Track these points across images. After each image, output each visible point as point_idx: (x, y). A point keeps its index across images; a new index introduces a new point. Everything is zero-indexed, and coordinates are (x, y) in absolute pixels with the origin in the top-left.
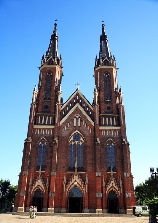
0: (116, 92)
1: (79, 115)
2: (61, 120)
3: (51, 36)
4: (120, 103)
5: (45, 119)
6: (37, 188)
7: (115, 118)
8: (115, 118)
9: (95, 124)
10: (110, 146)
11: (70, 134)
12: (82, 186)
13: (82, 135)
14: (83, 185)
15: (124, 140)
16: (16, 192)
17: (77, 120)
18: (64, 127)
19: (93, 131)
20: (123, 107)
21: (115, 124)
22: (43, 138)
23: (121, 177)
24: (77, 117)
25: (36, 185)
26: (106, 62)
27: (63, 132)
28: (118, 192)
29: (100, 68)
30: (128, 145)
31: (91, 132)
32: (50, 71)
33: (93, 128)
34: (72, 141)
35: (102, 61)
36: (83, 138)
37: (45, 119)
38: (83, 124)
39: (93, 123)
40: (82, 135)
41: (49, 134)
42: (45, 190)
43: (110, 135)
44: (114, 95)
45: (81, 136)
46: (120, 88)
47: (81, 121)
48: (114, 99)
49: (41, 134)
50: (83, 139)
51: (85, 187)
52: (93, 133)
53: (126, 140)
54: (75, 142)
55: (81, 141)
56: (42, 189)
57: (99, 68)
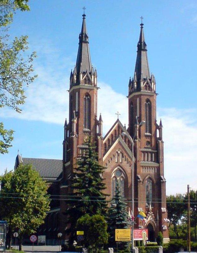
0: (96, 120)
2: (104, 155)
3: (79, 44)
4: (160, 138)
7: (153, 154)
8: (153, 154)
11: (113, 170)
13: (123, 171)
15: (162, 177)
16: (68, 222)
17: (118, 155)
20: (163, 142)
21: (153, 160)
22: (149, 176)
23: (158, 211)
24: (119, 152)
26: (147, 86)
28: (154, 224)
29: (134, 96)
30: (165, 182)
32: (87, 93)
35: (143, 85)
36: (123, 173)
40: (123, 171)
44: (93, 123)
45: (122, 172)
46: (100, 116)
47: (123, 156)
48: (153, 133)
50: (124, 175)
53: (164, 177)
56: (154, 223)
57: (139, 94)
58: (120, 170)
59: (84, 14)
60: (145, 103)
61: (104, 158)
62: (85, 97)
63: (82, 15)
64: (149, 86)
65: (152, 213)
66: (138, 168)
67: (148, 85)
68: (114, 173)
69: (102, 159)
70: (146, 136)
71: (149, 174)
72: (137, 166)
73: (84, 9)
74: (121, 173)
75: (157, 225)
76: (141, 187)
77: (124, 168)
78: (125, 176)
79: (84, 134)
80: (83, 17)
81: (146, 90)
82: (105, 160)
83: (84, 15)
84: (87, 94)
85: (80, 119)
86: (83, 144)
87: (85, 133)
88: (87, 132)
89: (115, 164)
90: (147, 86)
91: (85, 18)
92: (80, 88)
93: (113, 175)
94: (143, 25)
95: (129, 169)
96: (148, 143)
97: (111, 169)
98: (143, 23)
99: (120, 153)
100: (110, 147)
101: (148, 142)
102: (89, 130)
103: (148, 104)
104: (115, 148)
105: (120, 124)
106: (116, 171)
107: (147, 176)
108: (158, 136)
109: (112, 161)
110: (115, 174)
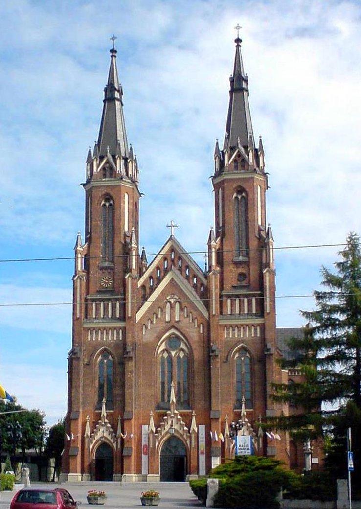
1: (175, 297)
5: (106, 309)
6: (100, 442)
9: (209, 314)
10: (243, 358)
12: (185, 436)
14: (185, 434)
17: (172, 307)
18: (146, 323)
19: (206, 330)
21: (254, 312)
24: (172, 301)
25: (97, 438)
27: (144, 333)
31: (201, 332)
32: (107, 194)
33: (206, 324)
34: (164, 351)
37: (106, 309)
38: (186, 316)
39: (206, 315)
41: (115, 339)
42: (115, 445)
43: (242, 336)
44: (254, 243)
45: (183, 340)
47: (181, 309)
49: (99, 339)
50: (187, 346)
51: (190, 437)
52: (206, 334)
54: (170, 353)
55: (182, 350)
58: (177, 337)
59: (113, 48)
60: (235, 195)
61: (139, 316)
62: (103, 202)
63: (234, 39)
64: (111, 168)
65: (246, 420)
66: (212, 329)
67: (240, 159)
68: (164, 343)
69: (133, 317)
70: (237, 264)
71: (242, 341)
72: (212, 326)
73: (114, 40)
74: (180, 343)
75: (117, 446)
76: (217, 367)
77: (184, 332)
78: (188, 348)
79: (101, 272)
80: (236, 44)
81: (237, 170)
82: (141, 319)
83: (238, 41)
84: (239, 189)
85: (92, 245)
86: (99, 292)
87: (104, 270)
88: (106, 268)
89: (164, 325)
90: (239, 160)
91: (240, 46)
92: (93, 187)
93: (163, 347)
94: (241, 41)
95: (195, 332)
96: (242, 276)
97: (155, 335)
98: (240, 38)
99: (175, 302)
100: (152, 290)
101: (241, 274)
102: (246, 259)
103: (243, 197)
104: (163, 293)
105: (174, 245)
106: (168, 338)
107: (236, 345)
108: (264, 261)
109: (157, 319)
110: (166, 344)
